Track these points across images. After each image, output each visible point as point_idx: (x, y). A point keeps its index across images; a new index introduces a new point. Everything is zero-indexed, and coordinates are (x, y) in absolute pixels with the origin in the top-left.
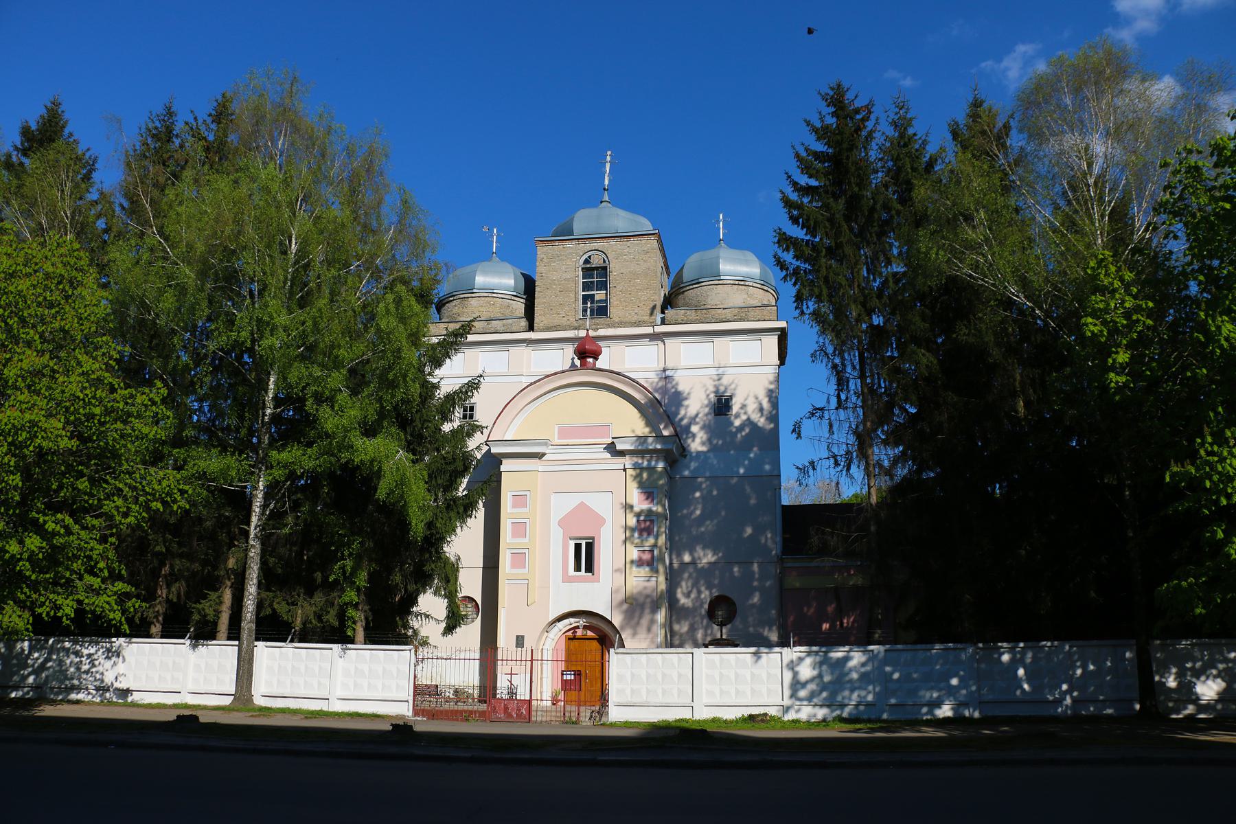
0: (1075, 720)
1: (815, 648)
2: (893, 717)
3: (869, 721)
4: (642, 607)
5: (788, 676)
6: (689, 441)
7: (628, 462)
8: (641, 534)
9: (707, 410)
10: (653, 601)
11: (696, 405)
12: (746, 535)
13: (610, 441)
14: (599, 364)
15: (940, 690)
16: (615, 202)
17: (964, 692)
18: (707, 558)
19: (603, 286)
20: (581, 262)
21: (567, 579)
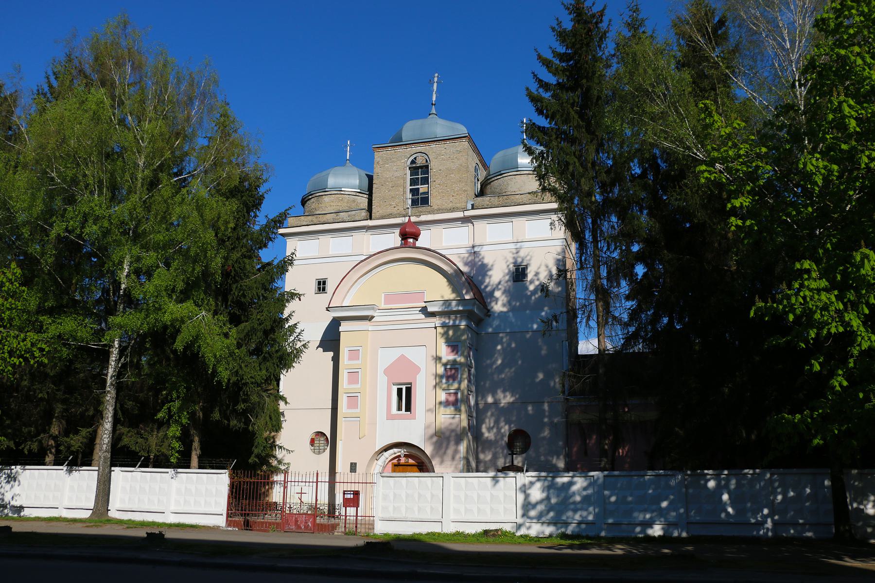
0: (777, 541)
1: (543, 474)
2: (610, 535)
3: (588, 538)
4: (448, 439)
5: (521, 497)
6: (493, 304)
7: (437, 321)
8: (447, 380)
9: (507, 278)
10: (457, 435)
11: (498, 275)
12: (538, 380)
13: (424, 305)
14: (418, 244)
15: (652, 512)
17: (674, 514)
18: (506, 399)
19: (425, 181)
20: (409, 163)
21: (390, 417)
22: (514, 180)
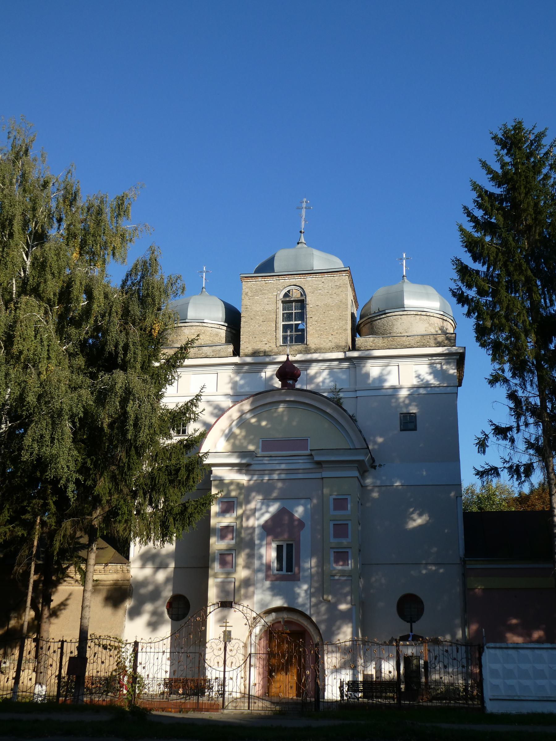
16: (310, 244)
20: (281, 296)
22: (400, 321)
